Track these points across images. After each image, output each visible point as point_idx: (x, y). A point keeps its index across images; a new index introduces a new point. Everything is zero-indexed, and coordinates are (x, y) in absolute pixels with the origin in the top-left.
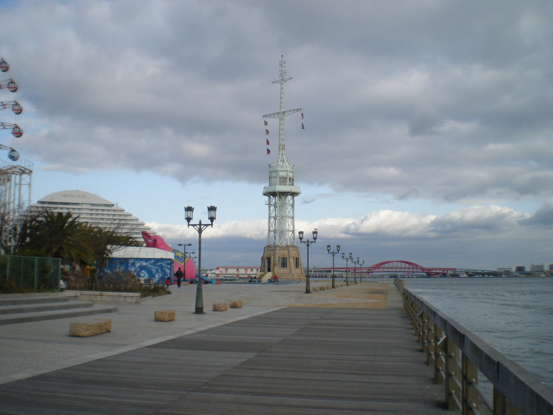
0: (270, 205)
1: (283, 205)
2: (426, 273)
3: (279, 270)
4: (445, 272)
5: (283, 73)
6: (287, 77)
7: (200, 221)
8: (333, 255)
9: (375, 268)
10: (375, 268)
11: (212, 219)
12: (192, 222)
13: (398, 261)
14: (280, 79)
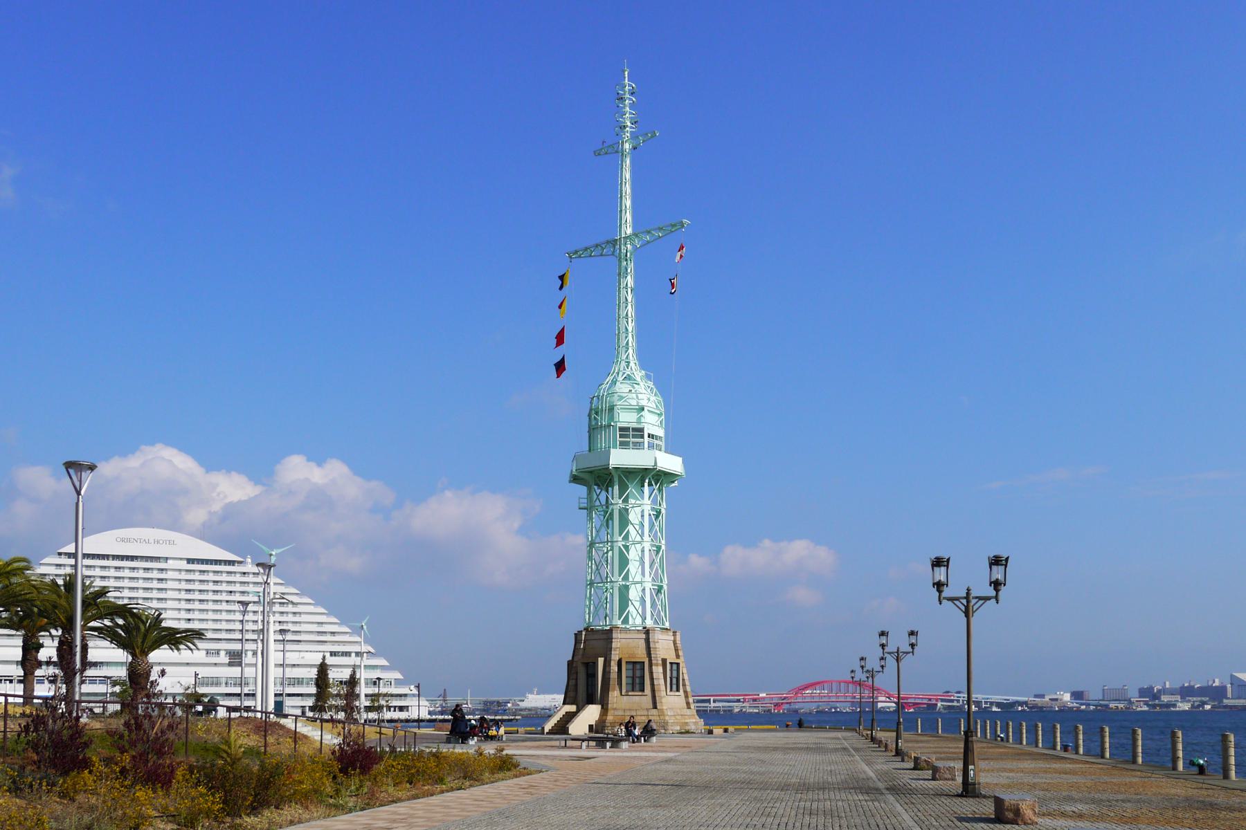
3: (622, 703)
12: (947, 592)
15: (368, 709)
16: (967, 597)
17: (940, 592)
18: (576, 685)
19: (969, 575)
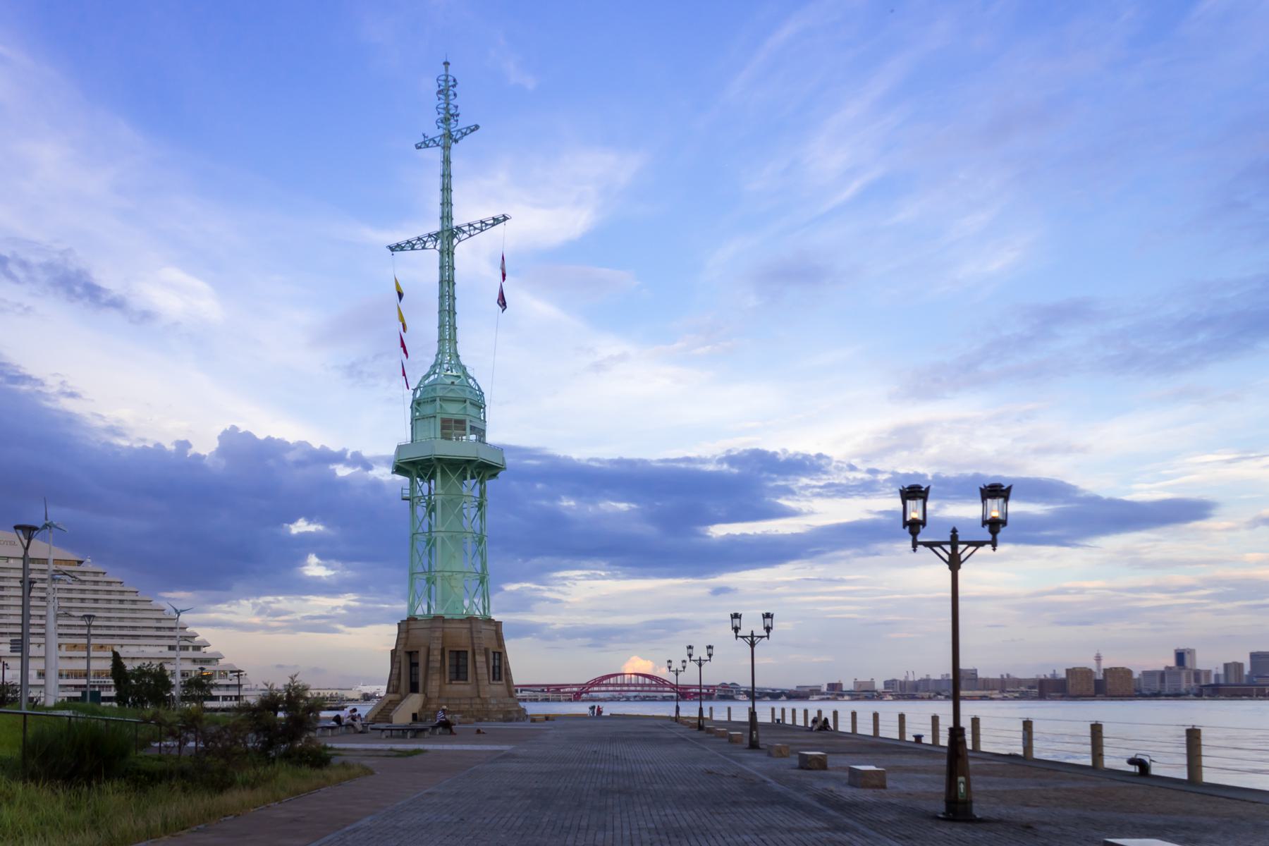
1: (453, 503)
5: (448, 117)
6: (463, 123)
7: (954, 531)
8: (752, 644)
9: (593, 685)
14: (441, 132)
15: (183, 699)
16: (752, 636)
17: (914, 533)
18: (400, 674)
19: (753, 623)
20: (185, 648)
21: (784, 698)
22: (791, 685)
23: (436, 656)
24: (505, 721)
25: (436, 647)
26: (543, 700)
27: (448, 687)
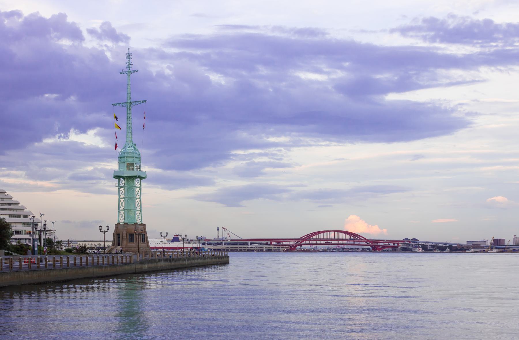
0: (119, 187)
2: (371, 246)
4: (396, 245)
9: (305, 239)
10: (305, 239)
11: (108, 230)
13: (335, 231)
20: (19, 216)
21: (448, 250)
22: (461, 240)
23: (125, 235)
24: (21, 239)
25: (125, 232)
26: (266, 251)
27: (128, 244)
